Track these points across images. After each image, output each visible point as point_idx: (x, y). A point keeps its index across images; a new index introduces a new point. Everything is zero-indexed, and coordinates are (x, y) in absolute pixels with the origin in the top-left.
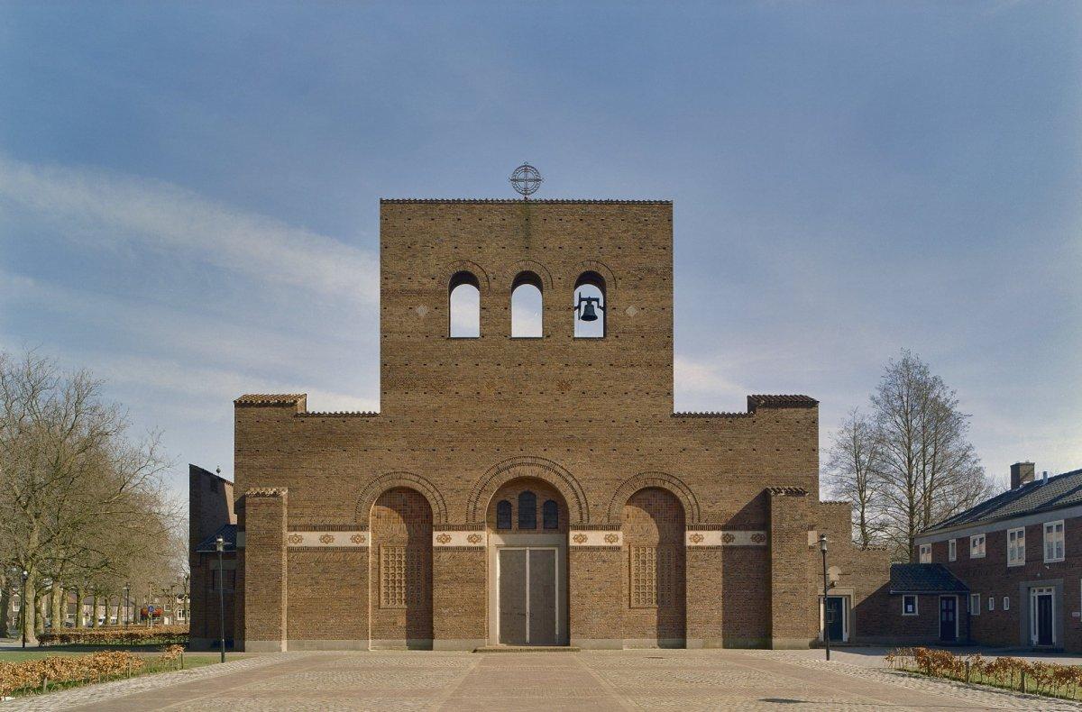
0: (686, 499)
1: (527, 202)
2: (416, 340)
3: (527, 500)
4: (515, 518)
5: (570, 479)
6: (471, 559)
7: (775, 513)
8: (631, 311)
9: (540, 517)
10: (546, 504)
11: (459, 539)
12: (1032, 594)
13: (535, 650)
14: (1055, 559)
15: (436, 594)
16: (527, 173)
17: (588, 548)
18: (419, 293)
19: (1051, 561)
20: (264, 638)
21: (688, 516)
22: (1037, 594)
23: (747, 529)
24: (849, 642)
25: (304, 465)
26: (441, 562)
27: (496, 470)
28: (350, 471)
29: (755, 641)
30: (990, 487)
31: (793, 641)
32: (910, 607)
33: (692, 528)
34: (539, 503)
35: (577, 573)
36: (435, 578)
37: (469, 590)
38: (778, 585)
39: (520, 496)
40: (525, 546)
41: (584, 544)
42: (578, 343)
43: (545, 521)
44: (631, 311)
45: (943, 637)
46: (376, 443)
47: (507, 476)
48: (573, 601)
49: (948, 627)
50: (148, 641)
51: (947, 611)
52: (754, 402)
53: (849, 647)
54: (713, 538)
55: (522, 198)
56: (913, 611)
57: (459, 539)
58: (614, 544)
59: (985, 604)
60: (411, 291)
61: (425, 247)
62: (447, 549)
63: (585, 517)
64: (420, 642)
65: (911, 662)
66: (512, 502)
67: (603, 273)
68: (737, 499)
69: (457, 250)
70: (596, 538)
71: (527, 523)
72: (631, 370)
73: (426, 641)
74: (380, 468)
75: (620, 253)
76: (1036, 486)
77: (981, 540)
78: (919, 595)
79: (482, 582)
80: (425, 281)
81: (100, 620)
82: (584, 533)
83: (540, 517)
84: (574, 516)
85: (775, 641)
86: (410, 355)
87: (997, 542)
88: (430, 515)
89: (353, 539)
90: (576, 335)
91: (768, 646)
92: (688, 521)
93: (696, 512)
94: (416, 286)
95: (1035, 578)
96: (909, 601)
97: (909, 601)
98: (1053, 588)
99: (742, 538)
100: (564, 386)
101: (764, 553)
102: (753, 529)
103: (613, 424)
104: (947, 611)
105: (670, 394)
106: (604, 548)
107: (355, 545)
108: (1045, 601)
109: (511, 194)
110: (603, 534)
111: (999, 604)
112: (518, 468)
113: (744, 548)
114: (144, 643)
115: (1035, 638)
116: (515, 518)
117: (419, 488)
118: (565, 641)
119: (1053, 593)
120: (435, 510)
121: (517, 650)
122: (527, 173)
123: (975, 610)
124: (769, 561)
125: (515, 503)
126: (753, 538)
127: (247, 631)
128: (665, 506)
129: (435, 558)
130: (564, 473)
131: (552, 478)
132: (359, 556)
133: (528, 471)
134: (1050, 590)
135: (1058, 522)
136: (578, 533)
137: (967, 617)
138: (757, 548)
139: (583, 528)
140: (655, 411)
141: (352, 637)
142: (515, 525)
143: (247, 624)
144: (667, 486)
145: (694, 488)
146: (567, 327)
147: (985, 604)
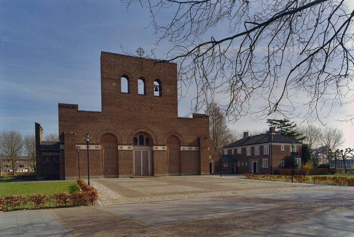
0: (181, 139)
1: (141, 58)
2: (112, 92)
3: (142, 137)
4: (138, 142)
5: (153, 133)
6: (128, 153)
7: (201, 142)
8: (168, 90)
9: (145, 142)
10: (146, 139)
11: (125, 148)
12: (252, 162)
13: (148, 177)
14: (257, 154)
15: (119, 163)
16: (140, 50)
17: (158, 151)
18: (113, 79)
19: (256, 155)
20: (71, 176)
21: (181, 143)
22: (253, 162)
23: (194, 146)
24: (213, 173)
25: (81, 126)
26: (121, 154)
27: (134, 130)
28: (94, 128)
29: (197, 174)
30: (52, 134)
31: (174, 174)
32: (226, 165)
33: (182, 146)
34: (144, 139)
35: (156, 157)
36: (119, 158)
37: (128, 162)
38: (202, 160)
39: (140, 136)
40: (141, 150)
41: (157, 150)
42: (155, 97)
43: (146, 143)
44: (168, 90)
45: (232, 172)
46: (102, 120)
47: (137, 131)
48: (155, 164)
49: (233, 169)
50: (7, 179)
51: (233, 166)
52: (195, 115)
53: (214, 174)
54: (186, 148)
55: (139, 56)
56: (226, 166)
57: (125, 148)
58: (164, 150)
59: (241, 164)
60: (111, 78)
61: (114, 66)
62: (122, 150)
63: (157, 143)
64: (178, 174)
65: (245, 177)
66: (137, 138)
67: (161, 80)
68: (192, 139)
69: (123, 69)
70: (160, 148)
71: (142, 144)
72: (168, 105)
73: (116, 176)
74: (103, 127)
75: (164, 74)
76: (250, 138)
77: (226, 151)
78: (228, 162)
79: (132, 159)
80: (114, 76)
81: (22, 170)
82: (157, 147)
83: (145, 142)
84: (155, 142)
85: (201, 173)
86: (109, 96)
87: (244, 150)
88: (117, 141)
89: (128, 148)
90: (122, 92)
91: (200, 175)
92: (181, 144)
93: (183, 142)
94: (112, 77)
95: (253, 158)
96: (226, 164)
97: (226, 164)
98: (257, 161)
99: (193, 149)
100: (152, 108)
101: (198, 153)
102: (196, 146)
103: (164, 119)
104: (233, 166)
105: (177, 112)
106: (162, 151)
107: (96, 149)
108: (255, 164)
109: (135, 54)
110: (162, 147)
111: (244, 164)
112: (140, 129)
113: (194, 151)
114: (5, 179)
115: (253, 171)
116: (138, 142)
117: (114, 133)
118: (152, 174)
119: (257, 162)
120: (119, 140)
121: (138, 177)
122: (140, 50)
123: (239, 165)
124: (200, 154)
125: (138, 138)
126: (196, 149)
127: (66, 174)
128: (175, 140)
129: (119, 153)
130: (152, 131)
131: (149, 132)
132: (97, 152)
133: (143, 130)
134: (256, 161)
135: (267, 146)
136: (156, 147)
137: (237, 167)
138: (197, 151)
139: (157, 146)
140: (173, 116)
141: (96, 175)
142: (138, 144)
143: (66, 172)
144: (176, 135)
145: (183, 136)
146: (152, 93)
147: (241, 164)
